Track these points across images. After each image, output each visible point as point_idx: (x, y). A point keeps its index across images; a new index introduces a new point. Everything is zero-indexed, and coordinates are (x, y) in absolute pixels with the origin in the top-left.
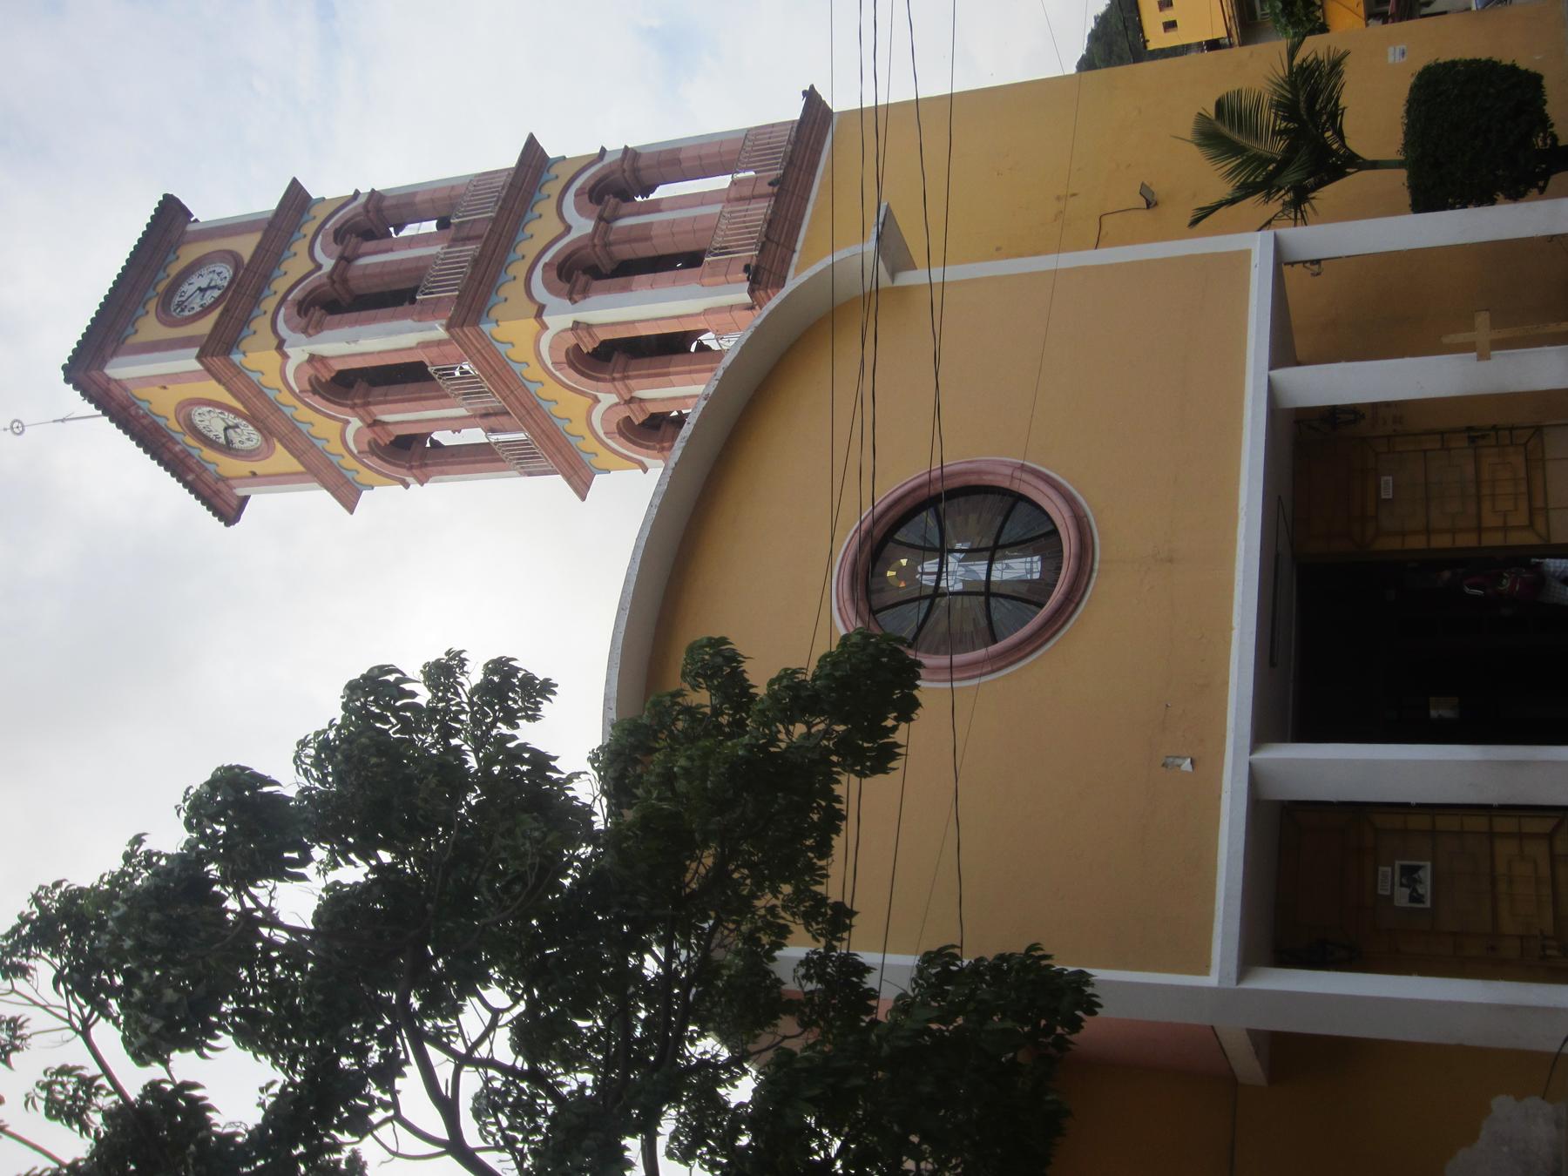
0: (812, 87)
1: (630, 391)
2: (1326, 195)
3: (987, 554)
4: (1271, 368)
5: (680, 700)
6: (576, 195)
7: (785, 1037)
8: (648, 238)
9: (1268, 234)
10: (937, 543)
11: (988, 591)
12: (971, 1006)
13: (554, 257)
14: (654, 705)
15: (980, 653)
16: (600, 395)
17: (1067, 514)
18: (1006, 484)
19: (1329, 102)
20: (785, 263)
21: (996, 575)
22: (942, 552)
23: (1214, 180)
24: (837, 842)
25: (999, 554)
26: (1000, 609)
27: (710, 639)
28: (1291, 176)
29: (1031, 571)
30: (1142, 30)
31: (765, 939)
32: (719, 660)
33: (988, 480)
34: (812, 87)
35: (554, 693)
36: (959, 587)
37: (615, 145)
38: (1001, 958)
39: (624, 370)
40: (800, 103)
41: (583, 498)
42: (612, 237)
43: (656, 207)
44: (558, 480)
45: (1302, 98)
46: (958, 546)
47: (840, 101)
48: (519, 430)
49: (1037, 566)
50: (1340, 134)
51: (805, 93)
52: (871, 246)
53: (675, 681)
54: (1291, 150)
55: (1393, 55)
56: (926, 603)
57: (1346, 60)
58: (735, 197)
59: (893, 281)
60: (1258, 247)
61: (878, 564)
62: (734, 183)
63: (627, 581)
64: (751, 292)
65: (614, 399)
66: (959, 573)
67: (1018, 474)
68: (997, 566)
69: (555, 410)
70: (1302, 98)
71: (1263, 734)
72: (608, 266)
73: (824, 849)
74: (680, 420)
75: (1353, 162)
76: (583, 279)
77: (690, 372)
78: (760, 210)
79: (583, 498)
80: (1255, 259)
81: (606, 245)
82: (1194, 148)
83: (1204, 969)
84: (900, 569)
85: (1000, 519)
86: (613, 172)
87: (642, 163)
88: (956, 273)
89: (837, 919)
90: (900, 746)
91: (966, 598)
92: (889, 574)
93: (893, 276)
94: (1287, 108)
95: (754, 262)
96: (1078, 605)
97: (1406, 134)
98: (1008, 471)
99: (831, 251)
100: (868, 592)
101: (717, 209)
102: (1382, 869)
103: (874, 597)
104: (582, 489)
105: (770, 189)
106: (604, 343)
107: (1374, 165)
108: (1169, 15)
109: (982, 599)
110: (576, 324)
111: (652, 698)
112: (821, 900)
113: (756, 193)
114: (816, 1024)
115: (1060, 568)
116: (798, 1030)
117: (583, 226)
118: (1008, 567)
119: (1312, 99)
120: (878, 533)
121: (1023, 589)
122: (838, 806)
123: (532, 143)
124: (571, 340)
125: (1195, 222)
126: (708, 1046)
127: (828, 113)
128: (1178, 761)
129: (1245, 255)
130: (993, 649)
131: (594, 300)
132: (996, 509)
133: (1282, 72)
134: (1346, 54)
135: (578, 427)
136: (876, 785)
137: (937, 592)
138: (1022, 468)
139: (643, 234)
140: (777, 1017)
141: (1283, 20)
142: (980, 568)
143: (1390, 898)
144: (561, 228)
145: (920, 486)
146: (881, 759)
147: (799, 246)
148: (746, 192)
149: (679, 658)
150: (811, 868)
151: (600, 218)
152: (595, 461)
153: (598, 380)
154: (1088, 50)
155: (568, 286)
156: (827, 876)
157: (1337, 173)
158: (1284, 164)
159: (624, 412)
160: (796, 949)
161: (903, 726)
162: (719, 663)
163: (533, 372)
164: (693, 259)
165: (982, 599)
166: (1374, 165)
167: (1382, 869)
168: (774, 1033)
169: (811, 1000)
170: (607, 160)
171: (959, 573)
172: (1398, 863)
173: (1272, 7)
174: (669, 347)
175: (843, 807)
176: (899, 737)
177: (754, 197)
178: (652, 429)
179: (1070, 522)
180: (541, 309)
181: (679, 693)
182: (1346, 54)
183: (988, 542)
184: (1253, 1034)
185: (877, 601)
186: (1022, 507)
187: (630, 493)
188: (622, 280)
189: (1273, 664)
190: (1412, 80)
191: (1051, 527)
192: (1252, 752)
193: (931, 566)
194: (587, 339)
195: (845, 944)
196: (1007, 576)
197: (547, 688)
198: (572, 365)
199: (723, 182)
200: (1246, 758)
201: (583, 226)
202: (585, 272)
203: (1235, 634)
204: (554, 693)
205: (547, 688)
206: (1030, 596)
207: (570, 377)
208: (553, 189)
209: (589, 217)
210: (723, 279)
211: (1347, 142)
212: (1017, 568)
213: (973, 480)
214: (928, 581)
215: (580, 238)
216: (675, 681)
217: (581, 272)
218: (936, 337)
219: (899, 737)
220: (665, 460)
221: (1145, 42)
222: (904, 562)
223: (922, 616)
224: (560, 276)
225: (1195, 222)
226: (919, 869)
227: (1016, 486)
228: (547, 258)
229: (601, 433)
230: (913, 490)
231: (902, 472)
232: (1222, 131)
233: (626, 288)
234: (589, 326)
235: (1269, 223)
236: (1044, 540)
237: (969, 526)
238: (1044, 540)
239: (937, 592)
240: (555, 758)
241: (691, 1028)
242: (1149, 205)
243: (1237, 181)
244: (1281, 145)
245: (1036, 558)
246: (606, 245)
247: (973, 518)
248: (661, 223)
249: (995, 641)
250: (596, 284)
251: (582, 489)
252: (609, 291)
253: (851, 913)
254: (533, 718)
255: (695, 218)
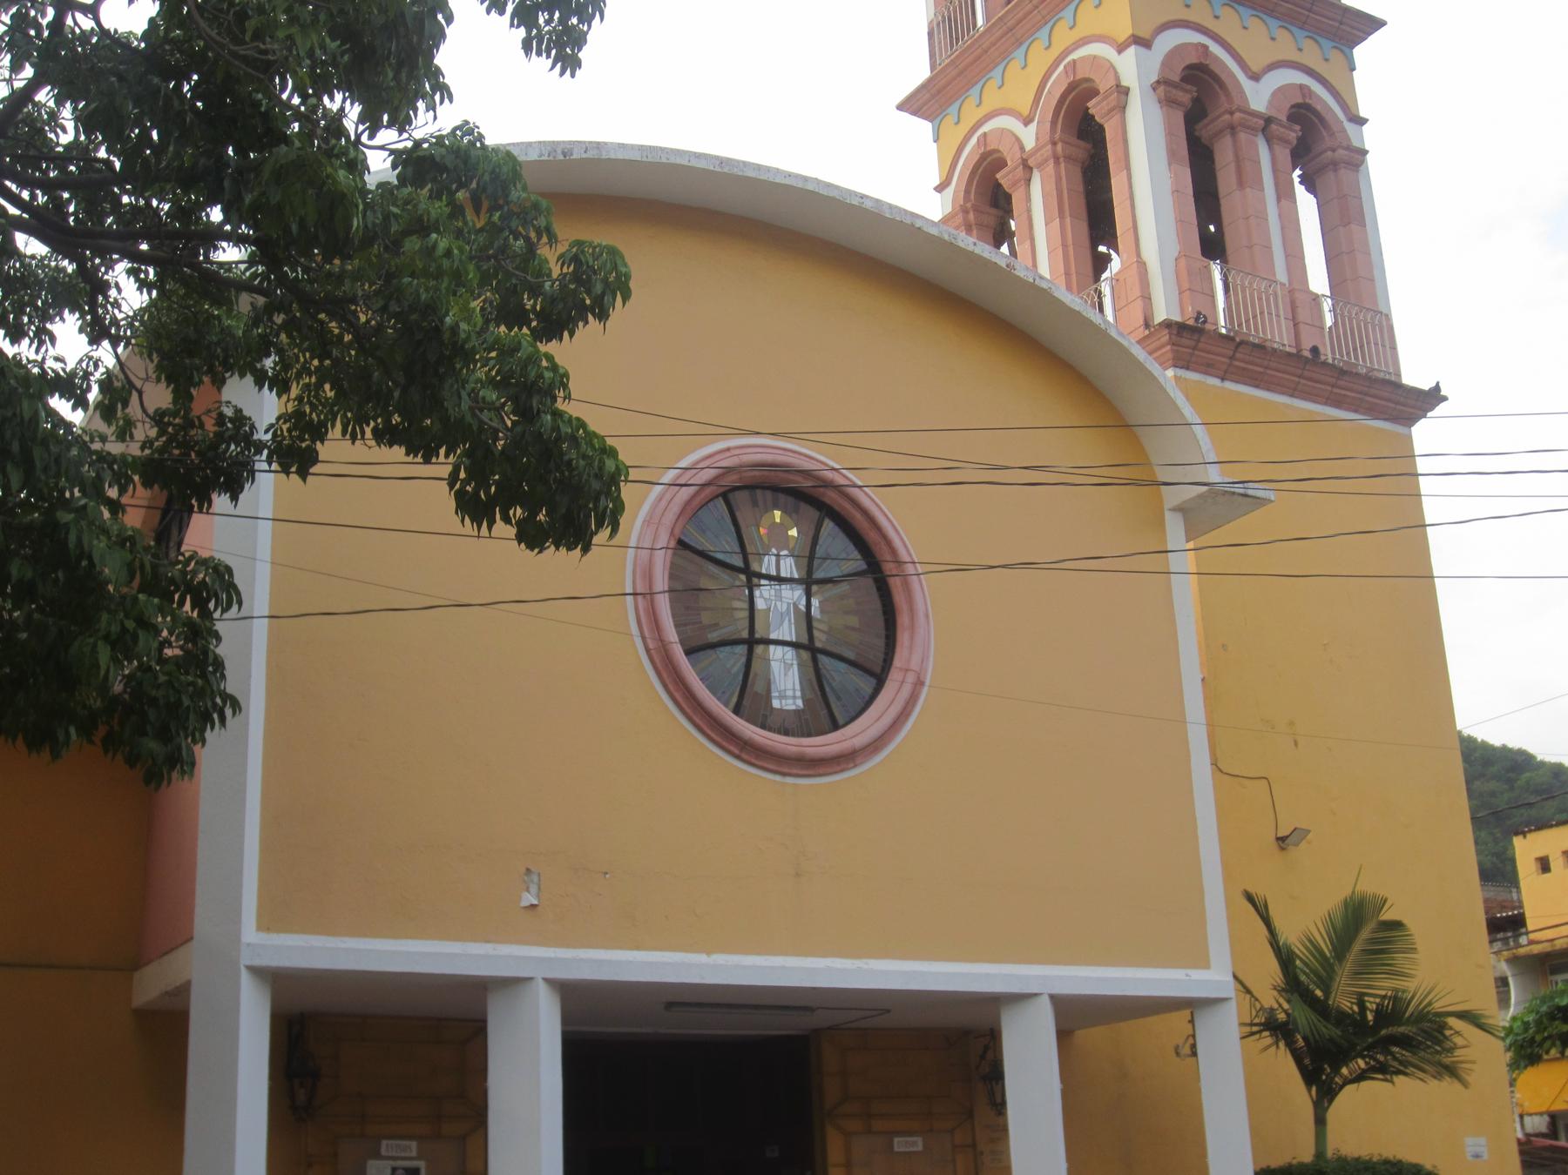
0: (1445, 399)
1: (1039, 166)
2: (1283, 1065)
3: (805, 640)
4: (1052, 997)
5: (545, 239)
6: (1301, 87)
7: (140, 393)
8: (1241, 184)
9: (1228, 989)
10: (819, 575)
11: (753, 642)
12: (130, 625)
13: (1217, 58)
14: (536, 206)
15: (671, 634)
16: (1033, 127)
17: (858, 742)
18: (898, 662)
19: (1401, 1063)
20: (1207, 368)
21: (776, 652)
22: (808, 582)
23: (1305, 921)
24: (398, 452)
25: (805, 655)
26: (733, 659)
27: (628, 276)
28: (1304, 1017)
29: (782, 697)
30: (1539, 828)
31: (269, 363)
32: (599, 288)
33: (903, 638)
34: (1445, 399)
35: (562, 73)
36: (760, 604)
37: (1370, 137)
38: (219, 664)
39: (1068, 158)
40: (1426, 385)
41: (900, 107)
42: (1243, 136)
43: (1285, 194)
44: (925, 73)
45: (1402, 1029)
46: (815, 602)
47: (1424, 434)
48: (988, 17)
49: (790, 705)
50: (1361, 1077)
51: (1437, 388)
52: (1214, 475)
53: (569, 232)
54: (1341, 1018)
55: (1475, 1144)
56: (737, 561)
57: (1457, 1086)
58: (1298, 298)
59: (1174, 510)
60: (1212, 978)
61: (791, 500)
62: (1316, 299)
63: (759, 167)
64: (1167, 324)
65: (1029, 143)
66: (779, 606)
67: (911, 678)
68: (790, 653)
69: (1015, 65)
70: (1402, 1029)
71: (572, 995)
72: (1204, 131)
73: (386, 436)
74: (1001, 235)
75: (1325, 1093)
76: (1185, 98)
77: (1065, 246)
78: (1279, 335)
79: (900, 107)
80: (1197, 974)
81: (1232, 128)
82: (1347, 892)
83: (265, 925)
84: (784, 528)
85: (850, 655)
86: (1332, 135)
87: (1344, 173)
88: (1185, 594)
89: (296, 455)
90: (490, 529)
91: (746, 614)
92: (777, 513)
93: (1179, 509)
94: (1392, 1011)
95: (1208, 327)
96: (738, 757)
97: (1357, 1159)
98: (914, 665)
99: (1204, 428)
100: (751, 487)
101: (1281, 275)
102: (414, 1144)
103: (744, 494)
104: (915, 104)
105: (1307, 345)
106: (1101, 129)
107: (1320, 1121)
108: (1556, 863)
109: (745, 634)
110: (1126, 91)
111: (544, 203)
112: (319, 433)
113: (1302, 326)
114: (162, 433)
115: (786, 733)
116: (151, 411)
117: (1259, 96)
118: (788, 667)
119: (1405, 1042)
120: (831, 497)
121: (759, 687)
122: (442, 451)
123: (1372, 24)
124: (1103, 85)
125: (1250, 898)
126: (129, 294)
127: (1411, 420)
128: (534, 889)
129: (1206, 965)
130: (678, 652)
131: (1157, 113)
132: (863, 651)
133: (1438, 1006)
134: (1465, 1084)
135: (993, 97)
136: (446, 500)
137: (752, 577)
138: (919, 683)
139: (1247, 177)
140: (169, 381)
141: (1544, 1009)
142: (786, 631)
143: (377, 1155)
144: (1255, 67)
145: (893, 551)
146: (475, 508)
147: (1229, 385)
148: (1303, 315)
149: (601, 235)
150: (362, 420)
151: (1269, 120)
152: (950, 120)
153: (1054, 123)
154: (1542, 763)
155: (1176, 78)
156: (354, 439)
157: (1310, 1076)
158: (1321, 1009)
159: (1012, 159)
160: (265, 409)
161: (511, 531)
162: (590, 292)
163: (1063, 35)
164: (1213, 247)
165: (745, 634)
166: (1320, 1121)
167: (414, 1144)
168: (147, 379)
169: (192, 426)
170: (1350, 127)
171: (779, 606)
172: (421, 1164)
173: (1563, 993)
174: (1097, 218)
175: (442, 458)
176: (500, 527)
177: (1296, 325)
178: (990, 197)
179: (846, 746)
180: (1144, 42)
181: (553, 239)
182: (1465, 1084)
183: (820, 640)
184: (184, 990)
185: (740, 498)
186: (865, 684)
187: (905, 175)
188: (1184, 151)
189: (670, 1005)
190: (1428, 1167)
191: (841, 722)
192: (550, 982)
193: (788, 568)
194: (1105, 106)
195: (265, 466)
196: (776, 667)
197: (568, 62)
198: (1072, 87)
199: (1318, 280)
200: (539, 974)
201: (1259, 96)
202: (1197, 101)
203: (702, 958)
204: (562, 73)
205: (568, 62)
206: (749, 695)
207: (1057, 84)
208: (1311, 56)
209: (1270, 103)
210: (1186, 285)
211: (1349, 1088)
212: (786, 680)
213: (903, 620)
214: (768, 565)
215: (1242, 92)
216: (569, 232)
217: (1196, 95)
218: (1056, 565)
219: (500, 527)
220: (945, 220)
221: (1524, 834)
222: (793, 532)
223: (720, 556)
224: (1189, 67)
225: (1250, 898)
226: (328, 552)
227: (894, 676)
228: (1215, 49)
229: (985, 128)
230: (889, 543)
231: (908, 524)
232: (1365, 930)
233: (1172, 156)
234: (1122, 108)
235: (1248, 991)
236: (825, 711)
237: (843, 615)
238: (825, 711)
239: (752, 577)
240: (573, 76)
241: (151, 271)
242: (1281, 840)
243: (1299, 949)
244: (1347, 1004)
245: (800, 703)
246: (1232, 128)
247: (853, 621)
248: (1263, 202)
249: (688, 653)
250: (1179, 117)
251: (915, 104)
252: (1170, 134)
253: (303, 474)
254: (527, 46)
255: (1269, 247)
